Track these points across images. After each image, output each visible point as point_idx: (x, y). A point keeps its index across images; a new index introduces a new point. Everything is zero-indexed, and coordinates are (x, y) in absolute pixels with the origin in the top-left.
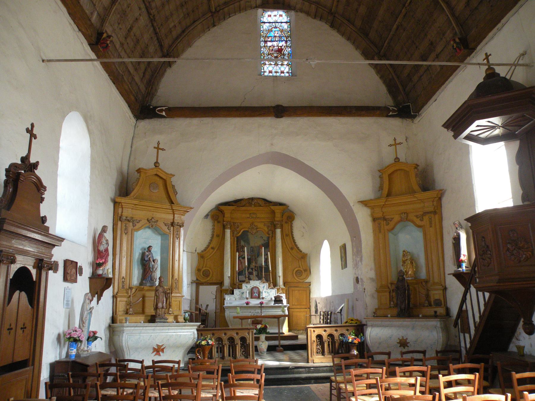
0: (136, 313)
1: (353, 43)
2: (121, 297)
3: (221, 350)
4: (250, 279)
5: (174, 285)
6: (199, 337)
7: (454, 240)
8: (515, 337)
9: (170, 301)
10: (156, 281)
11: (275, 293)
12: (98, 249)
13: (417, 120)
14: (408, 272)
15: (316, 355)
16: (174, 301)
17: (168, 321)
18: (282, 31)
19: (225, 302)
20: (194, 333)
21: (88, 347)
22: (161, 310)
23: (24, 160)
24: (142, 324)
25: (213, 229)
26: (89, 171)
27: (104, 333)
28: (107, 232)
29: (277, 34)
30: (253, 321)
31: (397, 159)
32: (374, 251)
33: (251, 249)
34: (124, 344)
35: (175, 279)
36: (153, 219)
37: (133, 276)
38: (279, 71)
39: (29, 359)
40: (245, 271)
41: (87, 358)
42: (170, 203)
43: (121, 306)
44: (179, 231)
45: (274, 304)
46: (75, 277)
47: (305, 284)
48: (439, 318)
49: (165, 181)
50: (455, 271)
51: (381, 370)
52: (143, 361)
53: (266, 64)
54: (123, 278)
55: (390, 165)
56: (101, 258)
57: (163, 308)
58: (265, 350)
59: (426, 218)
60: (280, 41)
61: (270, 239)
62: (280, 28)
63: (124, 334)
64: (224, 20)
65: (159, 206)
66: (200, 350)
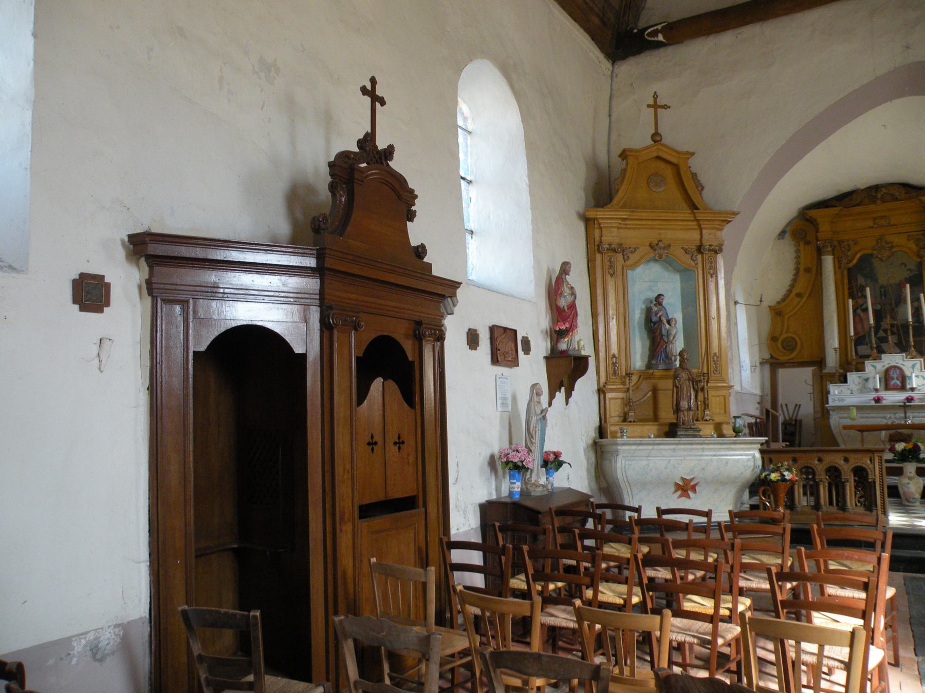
0: (643, 420)
2: (613, 390)
3: (812, 489)
4: (881, 351)
6: (766, 465)
9: (706, 396)
10: (675, 360)
16: (713, 396)
17: (701, 433)
20: (754, 456)
21: (547, 478)
22: (686, 413)
23: (367, 141)
24: (653, 439)
25: (798, 257)
27: (585, 454)
30: (891, 435)
33: (881, 292)
34: (619, 476)
35: (712, 355)
36: (660, 243)
37: (632, 352)
39: (418, 495)
40: (870, 336)
42: (690, 209)
43: (614, 410)
44: (713, 263)
46: (514, 356)
49: (676, 167)
52: (640, 507)
54: (614, 356)
57: (689, 409)
58: (918, 496)
65: (669, 216)
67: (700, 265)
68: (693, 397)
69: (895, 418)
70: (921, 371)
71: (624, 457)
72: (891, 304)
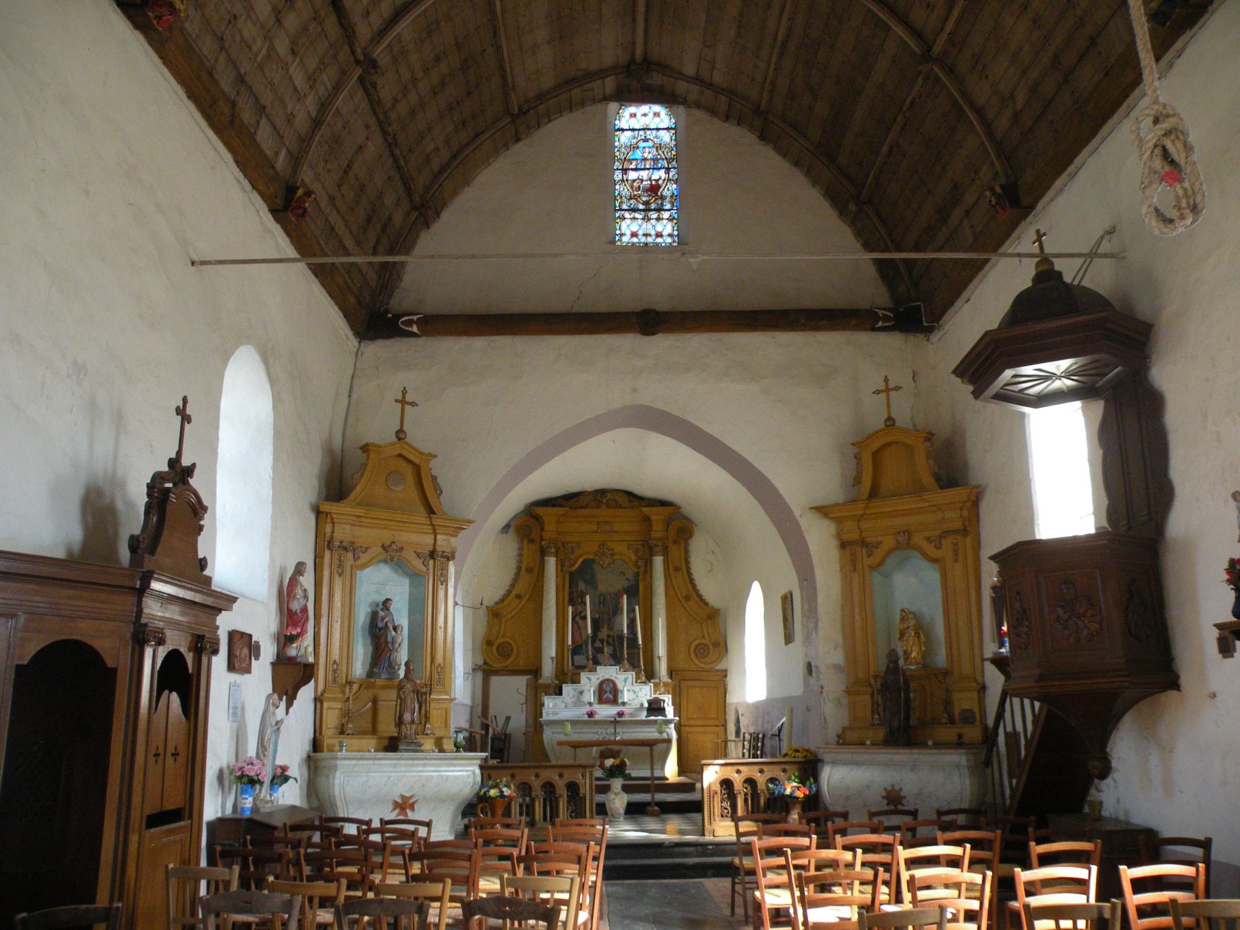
0: (360, 733)
1: (807, 174)
3: (529, 810)
5: (435, 676)
7: (994, 592)
8: (1093, 786)
10: (399, 669)
12: (288, 607)
13: (935, 337)
14: (911, 653)
15: (720, 821)
18: (658, 147)
19: (544, 712)
20: (474, 772)
23: (174, 463)
24: (373, 754)
25: (520, 555)
26: (271, 457)
27: (299, 770)
28: (305, 574)
29: (649, 153)
31: (890, 421)
32: (843, 610)
33: (600, 599)
34: (337, 793)
35: (437, 665)
38: (653, 232)
40: (587, 645)
41: (270, 814)
42: (427, 513)
43: (332, 718)
44: (445, 569)
45: (646, 717)
48: (965, 749)
50: (995, 653)
51: (851, 853)
53: (625, 219)
54: (335, 662)
55: (876, 432)
56: (295, 625)
57: (413, 722)
58: (622, 811)
59: (947, 544)
60: (654, 169)
61: (641, 577)
62: (655, 140)
63: (338, 774)
64: (539, 127)
66: (486, 807)
67: (431, 571)
68: (417, 710)
69: (607, 734)
71: (343, 773)
72: (609, 614)
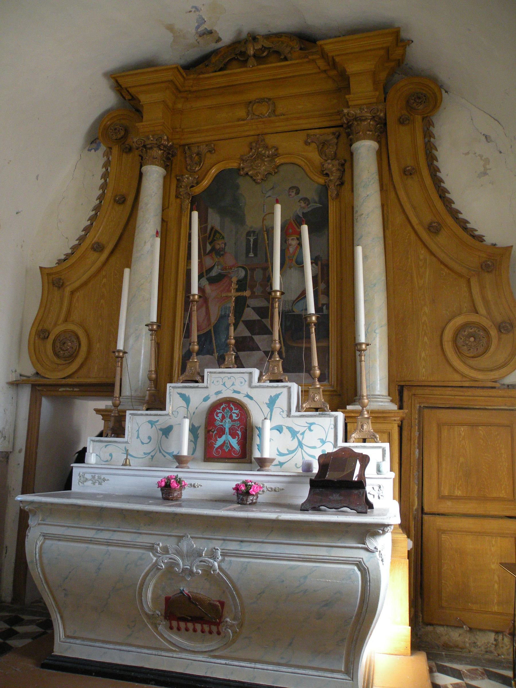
11: (331, 438)
33: (248, 241)
47: (500, 393)
61: (332, 192)
70: (289, 415)
